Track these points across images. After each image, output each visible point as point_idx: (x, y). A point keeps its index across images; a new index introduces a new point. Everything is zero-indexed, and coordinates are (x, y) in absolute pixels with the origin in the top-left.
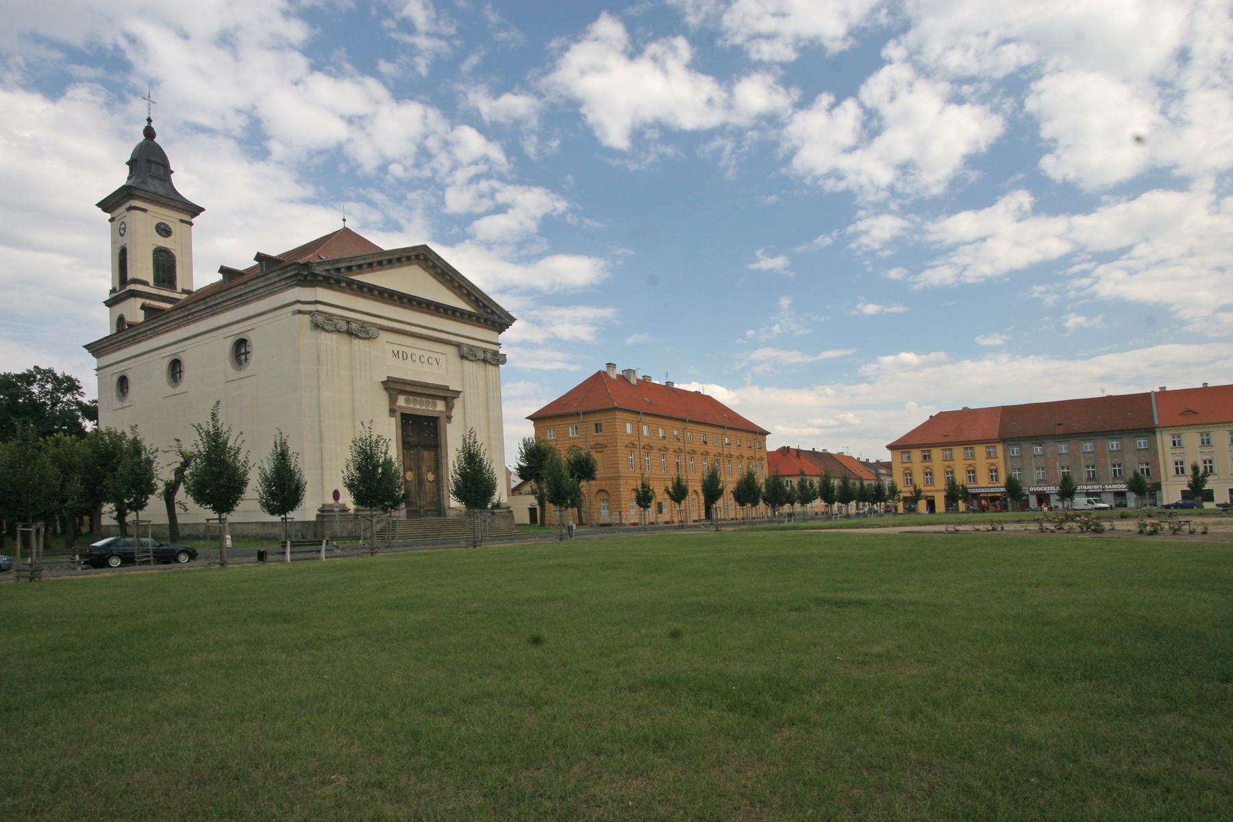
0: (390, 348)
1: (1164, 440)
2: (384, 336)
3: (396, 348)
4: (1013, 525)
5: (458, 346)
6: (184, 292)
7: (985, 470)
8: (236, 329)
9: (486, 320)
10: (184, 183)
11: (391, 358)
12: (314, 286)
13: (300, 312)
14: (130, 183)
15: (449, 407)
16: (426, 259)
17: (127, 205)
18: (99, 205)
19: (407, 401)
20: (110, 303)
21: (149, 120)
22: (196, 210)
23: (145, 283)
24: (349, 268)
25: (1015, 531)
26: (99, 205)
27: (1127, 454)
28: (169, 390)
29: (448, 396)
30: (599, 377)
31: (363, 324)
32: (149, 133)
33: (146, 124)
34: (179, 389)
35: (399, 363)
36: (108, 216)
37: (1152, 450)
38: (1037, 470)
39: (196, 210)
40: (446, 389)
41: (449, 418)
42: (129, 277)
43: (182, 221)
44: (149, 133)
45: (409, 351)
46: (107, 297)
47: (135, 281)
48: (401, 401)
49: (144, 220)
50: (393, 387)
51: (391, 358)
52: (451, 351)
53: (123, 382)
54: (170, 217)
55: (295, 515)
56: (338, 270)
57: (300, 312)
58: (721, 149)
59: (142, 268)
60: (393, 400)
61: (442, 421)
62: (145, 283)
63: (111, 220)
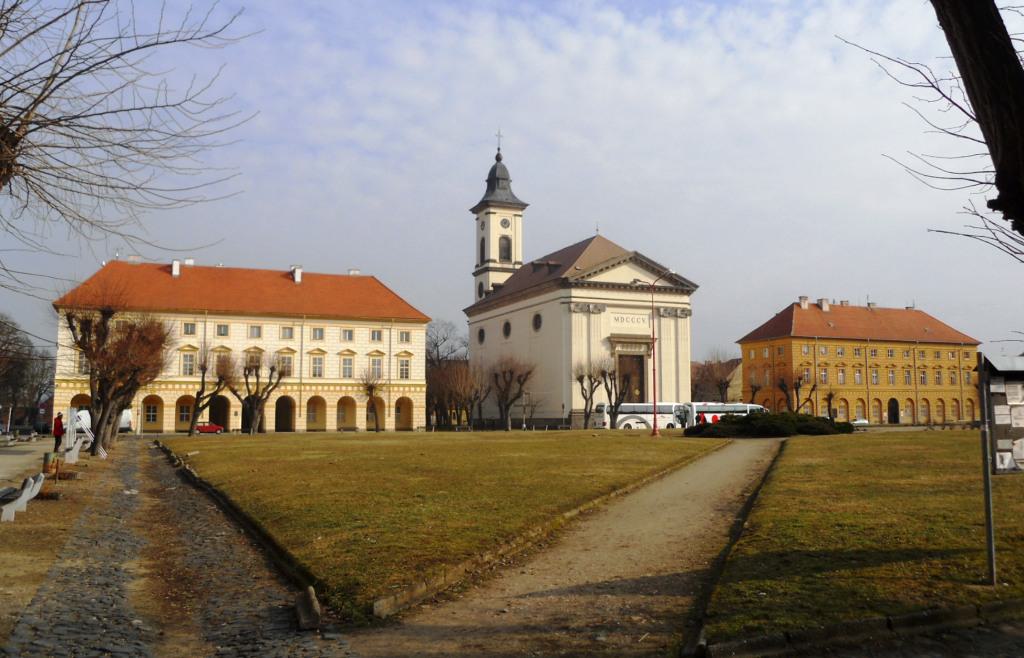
0: (613, 316)
2: (608, 309)
3: (617, 316)
6: (516, 263)
8: (535, 309)
9: (677, 290)
10: (518, 189)
11: (611, 323)
13: (563, 303)
16: (636, 260)
17: (485, 211)
18: (464, 310)
19: (623, 347)
20: (475, 274)
21: (499, 149)
23: (494, 261)
24: (589, 275)
25: (363, 448)
26: (464, 310)
28: (504, 340)
29: (649, 342)
31: (596, 305)
32: (498, 158)
33: (497, 152)
34: (508, 340)
35: (619, 324)
36: (475, 216)
39: (522, 206)
42: (486, 258)
43: (516, 215)
44: (498, 158)
45: (625, 316)
46: (474, 270)
47: (489, 261)
48: (619, 348)
53: (481, 335)
54: (507, 214)
56: (583, 277)
57: (563, 303)
59: (494, 252)
60: (613, 348)
61: (645, 358)
62: (494, 261)
63: (477, 219)
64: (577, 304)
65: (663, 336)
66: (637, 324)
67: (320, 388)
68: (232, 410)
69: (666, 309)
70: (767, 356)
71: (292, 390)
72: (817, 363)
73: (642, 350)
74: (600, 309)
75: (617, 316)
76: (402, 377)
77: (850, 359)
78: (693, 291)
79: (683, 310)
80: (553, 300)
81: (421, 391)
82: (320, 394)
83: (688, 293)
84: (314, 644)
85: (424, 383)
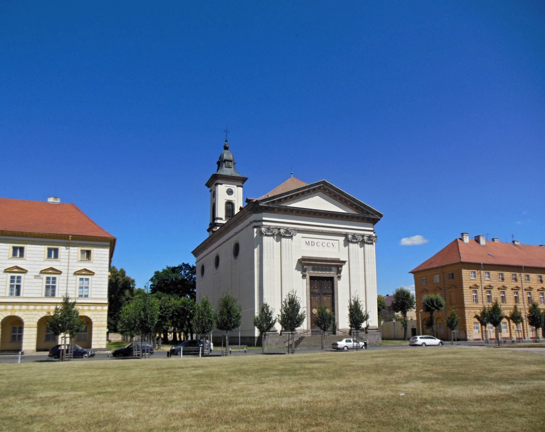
2: (299, 235)
5: (346, 235)
11: (303, 246)
12: (261, 212)
15: (339, 272)
23: (221, 219)
29: (337, 265)
31: (287, 231)
35: (310, 248)
40: (338, 261)
41: (339, 277)
50: (304, 264)
51: (303, 246)
61: (336, 279)
62: (221, 219)
63: (211, 191)
64: (269, 229)
65: (351, 259)
66: (328, 248)
67: (17, 307)
68: (95, 330)
69: (354, 236)
70: (438, 281)
71: (20, 310)
72: (524, 288)
73: (332, 274)
74: (289, 234)
75: (307, 240)
76: (11, 294)
77: (509, 283)
78: (379, 220)
79: (370, 237)
80: (247, 226)
81: (102, 310)
82: (17, 314)
83: (374, 221)
84: (299, 274)
85: (106, 302)
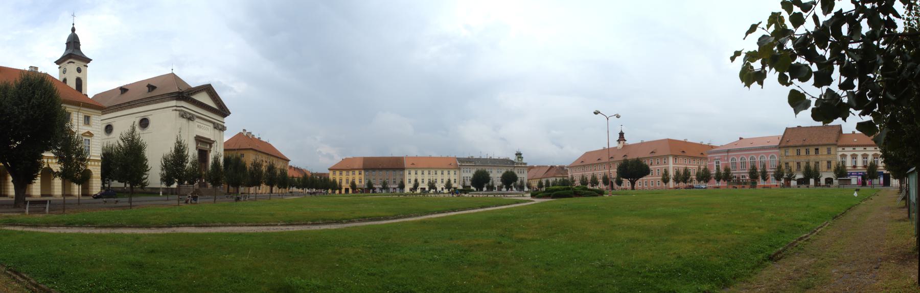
1: (407, 172)
2: (197, 120)
4: (369, 197)
5: (214, 123)
7: (360, 179)
8: (143, 114)
14: (69, 52)
15: (211, 146)
22: (89, 60)
27: (397, 175)
30: (240, 134)
31: (193, 115)
32: (73, 30)
37: (403, 175)
38: (377, 179)
39: (89, 60)
44: (73, 30)
49: (72, 68)
52: (212, 125)
54: (78, 64)
55: (172, 186)
58: (825, 13)
